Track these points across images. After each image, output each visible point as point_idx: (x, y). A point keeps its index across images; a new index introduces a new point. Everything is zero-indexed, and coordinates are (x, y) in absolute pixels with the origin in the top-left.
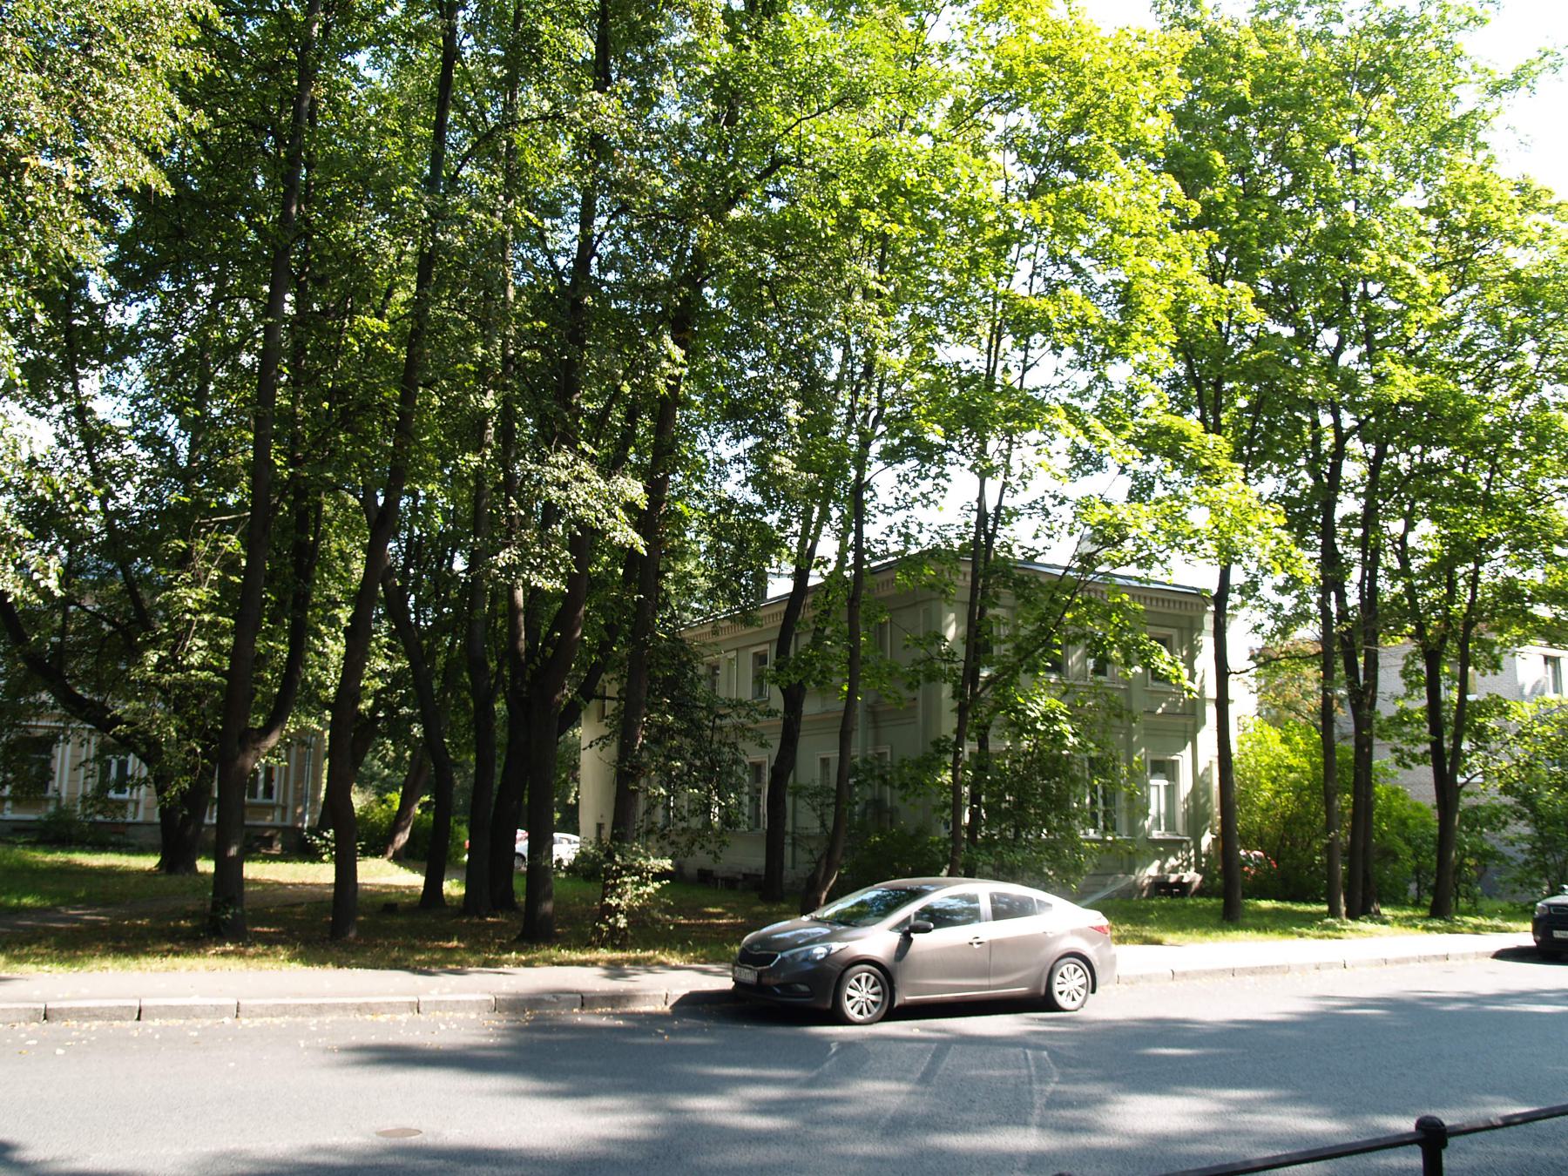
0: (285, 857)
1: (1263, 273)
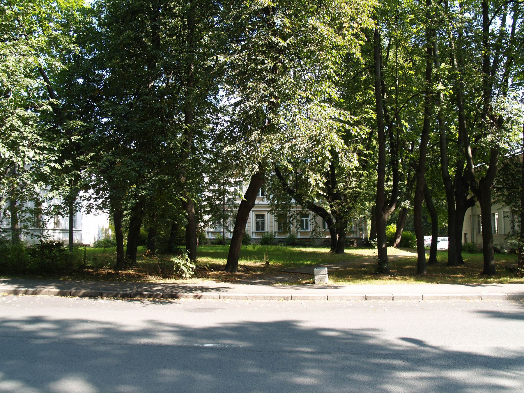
0: (356, 248)
1: (481, 30)
